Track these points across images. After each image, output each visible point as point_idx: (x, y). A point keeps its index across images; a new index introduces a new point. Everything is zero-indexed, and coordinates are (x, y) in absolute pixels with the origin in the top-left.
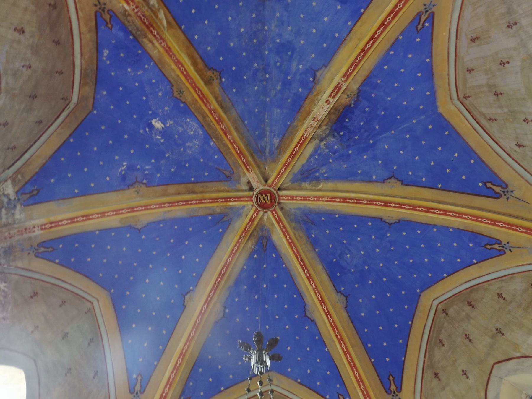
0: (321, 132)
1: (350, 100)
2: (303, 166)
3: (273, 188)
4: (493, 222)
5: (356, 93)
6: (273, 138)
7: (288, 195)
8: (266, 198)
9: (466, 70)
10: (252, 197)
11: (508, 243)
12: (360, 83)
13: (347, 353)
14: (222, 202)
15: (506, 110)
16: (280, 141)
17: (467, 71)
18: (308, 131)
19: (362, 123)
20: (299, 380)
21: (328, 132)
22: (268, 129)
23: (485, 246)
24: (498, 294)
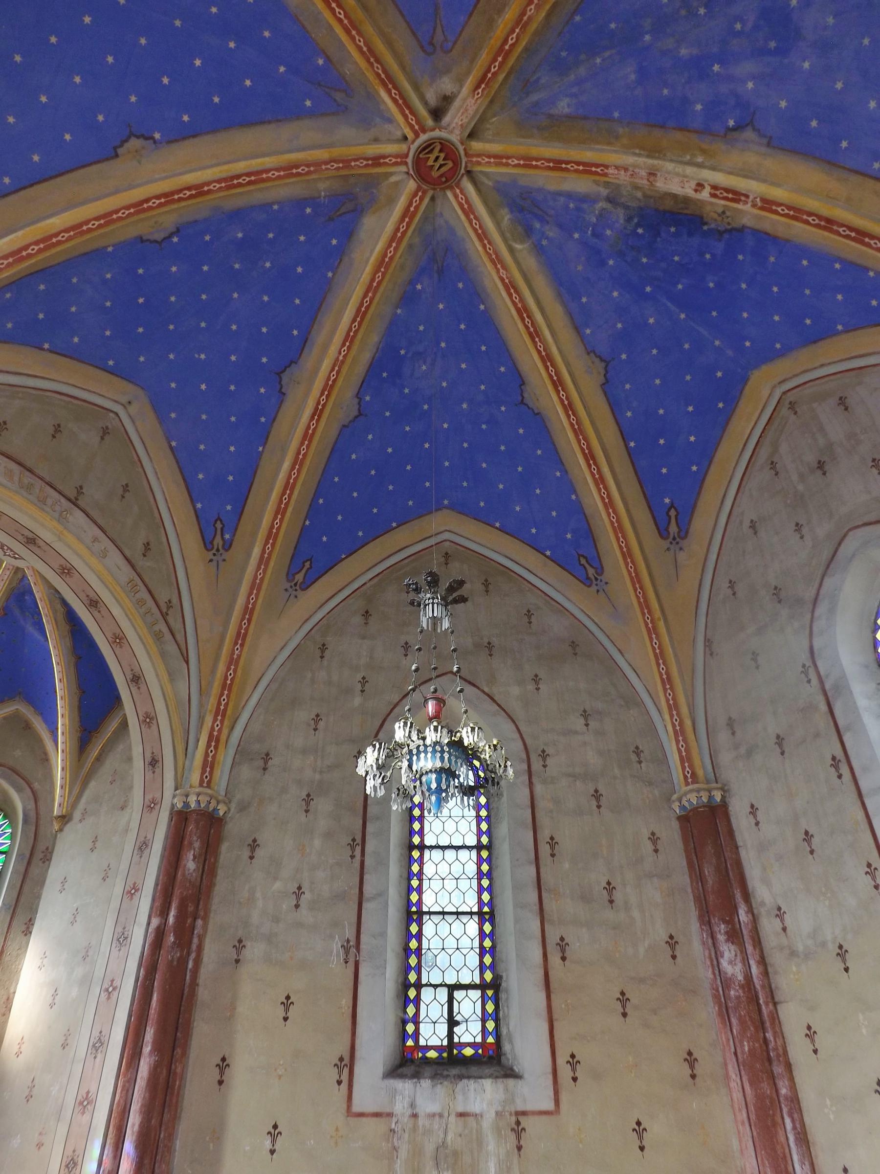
0: (628, 191)
1: (716, 220)
2: (540, 190)
3: (466, 163)
4: (627, 555)
5: (734, 225)
6: (567, 96)
7: (470, 199)
8: (441, 161)
9: (841, 395)
10: (424, 130)
11: (606, 583)
12: (757, 227)
13: (288, 486)
14: (378, 75)
15: (801, 487)
16: (568, 117)
17: (841, 398)
18: (622, 172)
19: (676, 258)
20: (174, 444)
21: (634, 204)
22: (582, 71)
23: (579, 556)
24: (529, 611)
